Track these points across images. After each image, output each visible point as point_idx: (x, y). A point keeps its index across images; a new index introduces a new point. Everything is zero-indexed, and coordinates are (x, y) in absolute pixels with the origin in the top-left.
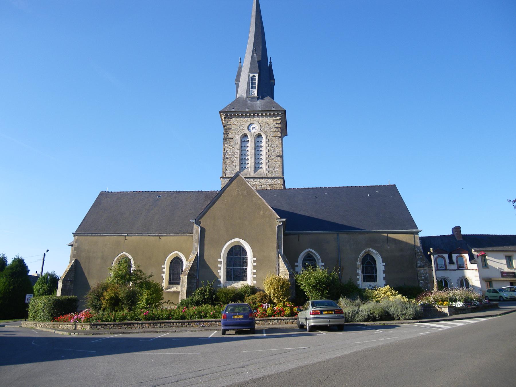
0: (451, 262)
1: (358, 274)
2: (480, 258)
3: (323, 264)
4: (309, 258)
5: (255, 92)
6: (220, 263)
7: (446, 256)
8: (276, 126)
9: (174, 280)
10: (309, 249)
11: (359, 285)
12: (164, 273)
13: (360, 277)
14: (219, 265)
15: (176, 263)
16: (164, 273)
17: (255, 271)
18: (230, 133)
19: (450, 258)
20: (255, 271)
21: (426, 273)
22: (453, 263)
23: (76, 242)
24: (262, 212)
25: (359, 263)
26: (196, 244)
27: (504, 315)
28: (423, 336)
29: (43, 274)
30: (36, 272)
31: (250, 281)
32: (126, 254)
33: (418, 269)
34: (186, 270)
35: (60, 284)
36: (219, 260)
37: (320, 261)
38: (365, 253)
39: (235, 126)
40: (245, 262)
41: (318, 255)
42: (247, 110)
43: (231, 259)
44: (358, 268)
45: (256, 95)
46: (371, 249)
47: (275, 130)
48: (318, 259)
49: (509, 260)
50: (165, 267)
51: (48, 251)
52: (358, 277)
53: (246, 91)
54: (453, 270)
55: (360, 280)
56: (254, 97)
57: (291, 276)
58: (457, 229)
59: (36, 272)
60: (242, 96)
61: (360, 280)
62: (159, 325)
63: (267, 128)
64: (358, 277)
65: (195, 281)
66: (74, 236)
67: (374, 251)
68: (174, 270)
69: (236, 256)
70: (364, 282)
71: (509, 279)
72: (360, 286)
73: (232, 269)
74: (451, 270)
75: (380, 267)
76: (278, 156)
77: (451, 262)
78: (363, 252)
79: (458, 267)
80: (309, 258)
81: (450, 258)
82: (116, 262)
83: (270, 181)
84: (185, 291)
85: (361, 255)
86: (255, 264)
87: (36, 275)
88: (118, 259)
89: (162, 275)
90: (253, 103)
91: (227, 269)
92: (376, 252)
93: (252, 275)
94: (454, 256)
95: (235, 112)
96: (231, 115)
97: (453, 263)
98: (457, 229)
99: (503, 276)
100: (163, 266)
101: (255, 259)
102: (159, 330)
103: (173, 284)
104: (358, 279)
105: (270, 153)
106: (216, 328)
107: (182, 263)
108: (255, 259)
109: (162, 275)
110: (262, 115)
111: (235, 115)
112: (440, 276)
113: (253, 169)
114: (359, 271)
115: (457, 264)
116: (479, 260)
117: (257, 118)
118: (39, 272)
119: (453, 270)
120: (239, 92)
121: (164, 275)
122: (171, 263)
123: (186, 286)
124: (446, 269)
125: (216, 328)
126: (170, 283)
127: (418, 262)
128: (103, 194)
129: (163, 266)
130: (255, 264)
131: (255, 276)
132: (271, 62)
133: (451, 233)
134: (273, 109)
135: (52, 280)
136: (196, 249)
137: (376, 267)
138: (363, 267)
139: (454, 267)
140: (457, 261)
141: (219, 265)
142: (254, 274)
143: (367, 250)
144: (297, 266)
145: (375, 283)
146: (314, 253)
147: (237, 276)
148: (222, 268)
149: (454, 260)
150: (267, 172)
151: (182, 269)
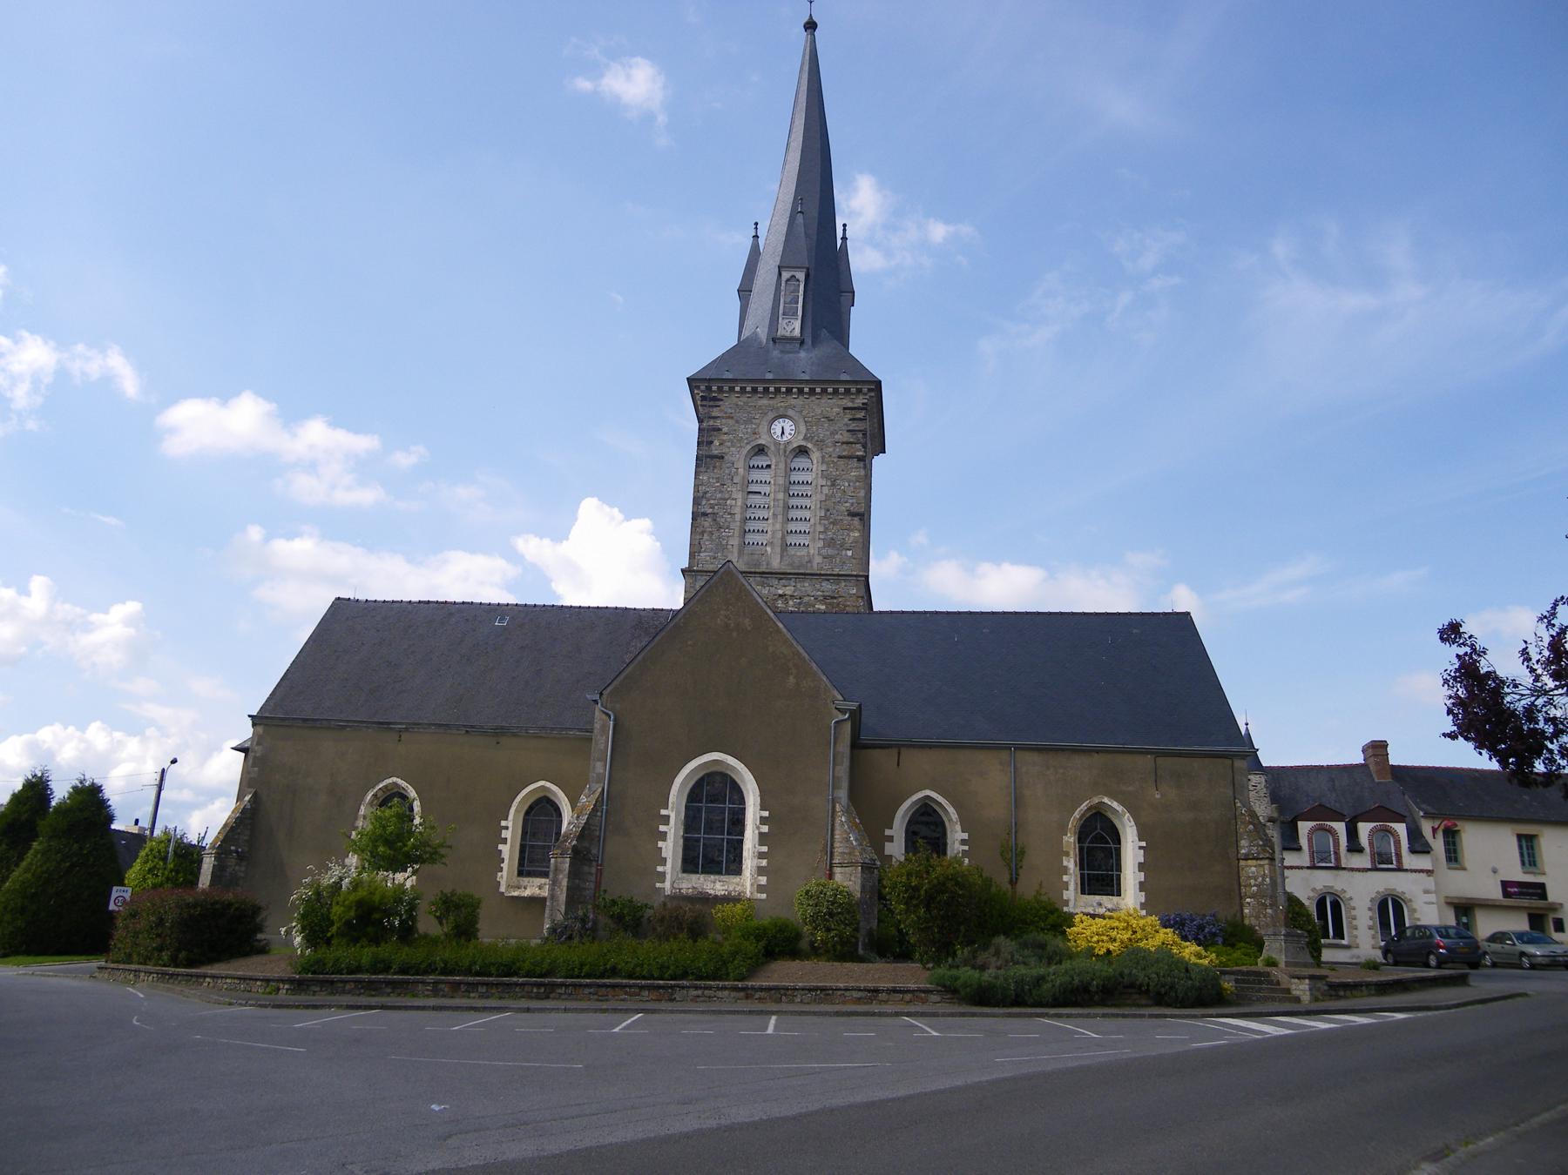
0: (1355, 847)
1: (1065, 870)
2: (1440, 835)
3: (965, 836)
4: (924, 819)
5: (794, 327)
6: (666, 820)
7: (1340, 827)
8: (853, 426)
9: (530, 864)
10: (928, 792)
11: (1066, 903)
12: (504, 841)
13: (1072, 877)
14: (662, 828)
15: (542, 812)
16: (504, 841)
17: (765, 849)
18: (717, 443)
19: (1352, 834)
20: (765, 849)
21: (1264, 876)
22: (1360, 850)
23: (258, 744)
24: (792, 680)
25: (1070, 839)
26: (599, 764)
27: (1480, 1006)
28: (1198, 1049)
29: (157, 833)
30: (137, 822)
31: (748, 881)
32: (399, 781)
33: (1242, 863)
34: (567, 836)
35: (208, 864)
36: (663, 812)
37: (958, 827)
38: (1089, 809)
39: (731, 422)
40: (738, 822)
41: (951, 810)
42: (770, 376)
43: (699, 810)
44: (1067, 854)
45: (797, 333)
46: (1106, 800)
47: (847, 437)
48: (950, 820)
49: (1528, 845)
50: (510, 824)
51: (174, 761)
52: (1065, 878)
53: (767, 322)
54: (1358, 870)
55: (1072, 887)
56: (792, 339)
57: (246, 829)
58: (1377, 749)
59: (137, 822)
60: (755, 333)
61: (1072, 887)
62: (482, 989)
63: (823, 432)
64: (1065, 878)
65: (593, 870)
66: (254, 725)
67: (1115, 805)
68: (534, 835)
69: (714, 808)
70: (1083, 892)
71: (1525, 902)
72: (1071, 904)
73: (698, 840)
74: (1352, 870)
75: (1131, 852)
76: (852, 514)
77: (1355, 847)
78: (1084, 806)
79: (1373, 862)
80: (924, 819)
81: (1352, 834)
82: (371, 803)
83: (827, 587)
84: (563, 897)
85: (1077, 814)
86: (765, 829)
87: (135, 830)
88: (375, 795)
89: (501, 847)
90: (786, 357)
91: (686, 840)
92: (1119, 808)
93: (756, 861)
94: (1364, 829)
95: (735, 380)
96: (720, 390)
97: (1360, 850)
98: (1377, 749)
99: (1506, 894)
100: (503, 823)
101: (766, 814)
102: (480, 1003)
103: (530, 874)
104: (1066, 886)
105: (829, 504)
106: (642, 1006)
107: (560, 815)
108: (766, 814)
109: (501, 847)
110: (812, 391)
111: (732, 389)
112: (1319, 887)
113: (778, 550)
114: (1070, 863)
115: (1372, 855)
116: (1438, 845)
117: (800, 401)
118: (145, 823)
119: (1358, 870)
120: (749, 323)
121: (505, 849)
122: (527, 813)
123: (565, 883)
124: (1338, 868)
125: (642, 1006)
126: (520, 874)
127: (1243, 843)
128: (341, 607)
129: (503, 823)
130: (765, 829)
131: (764, 863)
132: (844, 238)
133: (1359, 759)
134: (844, 377)
135: (188, 855)
136: (600, 779)
137: (1118, 851)
138: (1081, 849)
139: (1363, 861)
140: (1371, 844)
141: (662, 828)
142: (761, 856)
143: (1096, 800)
144: (891, 839)
145: (1115, 899)
146: (940, 804)
147: (713, 861)
148: (671, 837)
149: (1364, 840)
150: (818, 559)
151: (558, 833)
